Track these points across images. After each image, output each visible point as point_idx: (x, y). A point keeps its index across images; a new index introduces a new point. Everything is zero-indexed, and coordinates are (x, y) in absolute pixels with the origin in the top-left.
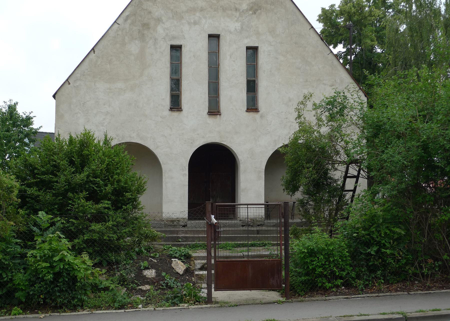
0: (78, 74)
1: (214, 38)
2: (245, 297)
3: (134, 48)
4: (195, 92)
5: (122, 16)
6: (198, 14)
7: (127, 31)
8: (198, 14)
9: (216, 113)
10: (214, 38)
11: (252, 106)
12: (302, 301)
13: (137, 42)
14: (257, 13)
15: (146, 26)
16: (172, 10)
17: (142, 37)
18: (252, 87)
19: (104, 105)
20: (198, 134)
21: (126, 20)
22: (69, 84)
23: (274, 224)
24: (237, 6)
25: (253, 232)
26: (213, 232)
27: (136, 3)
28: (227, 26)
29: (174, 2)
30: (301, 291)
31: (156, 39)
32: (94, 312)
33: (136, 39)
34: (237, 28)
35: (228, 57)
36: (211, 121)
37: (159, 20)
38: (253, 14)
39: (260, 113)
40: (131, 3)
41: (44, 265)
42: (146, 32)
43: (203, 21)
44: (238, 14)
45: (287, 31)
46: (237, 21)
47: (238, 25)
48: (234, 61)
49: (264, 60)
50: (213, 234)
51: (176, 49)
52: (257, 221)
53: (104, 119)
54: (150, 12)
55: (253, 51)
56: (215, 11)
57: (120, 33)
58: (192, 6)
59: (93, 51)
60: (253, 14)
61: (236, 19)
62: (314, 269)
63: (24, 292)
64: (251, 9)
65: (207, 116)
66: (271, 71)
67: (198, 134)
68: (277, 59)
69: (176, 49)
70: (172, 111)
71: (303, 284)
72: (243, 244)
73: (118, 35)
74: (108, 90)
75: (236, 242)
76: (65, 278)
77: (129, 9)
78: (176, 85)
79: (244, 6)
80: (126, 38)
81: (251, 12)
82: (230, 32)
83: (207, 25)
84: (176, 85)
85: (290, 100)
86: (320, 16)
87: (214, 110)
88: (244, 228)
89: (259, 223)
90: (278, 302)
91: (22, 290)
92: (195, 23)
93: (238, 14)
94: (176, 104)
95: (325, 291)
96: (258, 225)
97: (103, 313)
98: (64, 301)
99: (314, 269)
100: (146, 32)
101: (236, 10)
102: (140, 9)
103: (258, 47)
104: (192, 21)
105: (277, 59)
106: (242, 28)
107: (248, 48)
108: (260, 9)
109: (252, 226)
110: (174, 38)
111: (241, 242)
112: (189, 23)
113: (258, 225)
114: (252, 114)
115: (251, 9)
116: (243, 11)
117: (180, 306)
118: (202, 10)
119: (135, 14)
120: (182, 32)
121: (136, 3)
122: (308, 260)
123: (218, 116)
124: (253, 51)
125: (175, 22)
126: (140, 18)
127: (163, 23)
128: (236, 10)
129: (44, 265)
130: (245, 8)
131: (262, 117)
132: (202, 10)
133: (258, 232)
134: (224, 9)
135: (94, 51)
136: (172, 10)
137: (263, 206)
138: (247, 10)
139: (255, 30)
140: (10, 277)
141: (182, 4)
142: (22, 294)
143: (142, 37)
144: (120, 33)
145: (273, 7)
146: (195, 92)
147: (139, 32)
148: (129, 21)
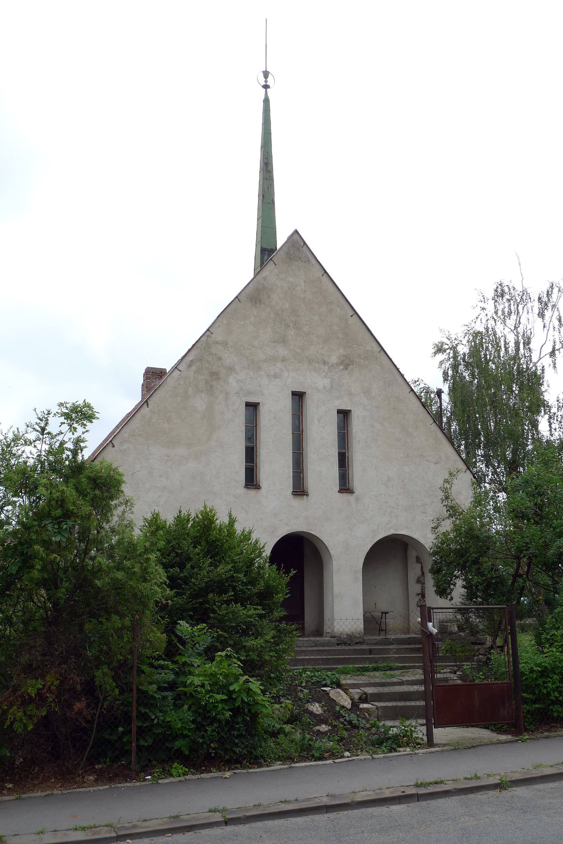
0: (125, 433)
1: (298, 397)
2: (476, 735)
3: (200, 403)
4: (275, 464)
5: (185, 360)
6: (279, 365)
7: (191, 381)
8: (279, 365)
9: (299, 493)
10: (298, 397)
11: (345, 487)
13: (203, 395)
14: (349, 369)
15: (215, 375)
16: (247, 358)
17: (210, 390)
18: (343, 460)
19: (160, 477)
20: (280, 520)
21: (190, 366)
22: (114, 446)
23: (376, 641)
24: (326, 358)
25: (363, 652)
26: (431, 645)
27: (202, 345)
28: (314, 382)
29: (249, 347)
30: (529, 725)
31: (227, 394)
32: (293, 765)
33: (202, 391)
34: (326, 385)
35: (316, 422)
36: (296, 502)
37: (231, 369)
38: (344, 369)
39: (355, 494)
40: (196, 345)
41: (219, 697)
42: (214, 383)
43: (286, 374)
44: (326, 368)
45: (384, 393)
46: (325, 377)
47: (327, 382)
48: (323, 427)
49: (357, 426)
50: (431, 648)
51: (252, 408)
52: (356, 637)
53: (160, 497)
54: (220, 359)
55: (344, 415)
56: (299, 362)
57: (182, 382)
58: (271, 355)
59: (146, 404)
60: (344, 369)
61: (324, 374)
62: (549, 694)
63: (187, 740)
64: (341, 364)
65: (292, 496)
66: (366, 442)
67: (280, 520)
68: (373, 427)
69: (252, 408)
70: (248, 488)
71: (532, 715)
72: (363, 667)
73: (179, 384)
74: (166, 458)
75: (355, 666)
76: (245, 717)
77: (193, 352)
78: (251, 454)
79: (334, 359)
80: (190, 389)
81: (342, 367)
82: (318, 391)
83: (289, 380)
84: (251, 454)
85: (389, 480)
87: (299, 490)
88: (339, 647)
89: (358, 641)
90: (511, 742)
91: (186, 736)
92: (276, 376)
93: (326, 368)
94: (252, 480)
96: (357, 643)
97: (306, 766)
98: (244, 751)
99: (549, 694)
100: (214, 383)
101: (324, 363)
102: (208, 353)
103: (350, 411)
104: (272, 373)
105: (373, 427)
106: (332, 386)
107: (339, 412)
108: (353, 365)
109: (350, 645)
110: (250, 393)
111: (361, 666)
112: (268, 376)
113: (357, 643)
114: (345, 496)
115: (341, 364)
116: (332, 365)
117: (400, 751)
118: (284, 360)
119: (201, 360)
120: (260, 386)
121: (202, 345)
122: (540, 681)
123: (305, 496)
124: (344, 415)
125: (251, 373)
126: (207, 365)
127: (237, 373)
128: (324, 363)
129: (219, 697)
130: (335, 362)
131: (357, 499)
132: (284, 360)
133: (371, 652)
134: (310, 362)
135: (147, 404)
136: (247, 358)
137: (451, 610)
138: (337, 364)
139: (346, 390)
140: (161, 718)
141: (259, 350)
142: (184, 742)
143: (210, 390)
144: (182, 382)
145: (367, 362)
146: (275, 464)
147: (207, 382)
148: (194, 368)
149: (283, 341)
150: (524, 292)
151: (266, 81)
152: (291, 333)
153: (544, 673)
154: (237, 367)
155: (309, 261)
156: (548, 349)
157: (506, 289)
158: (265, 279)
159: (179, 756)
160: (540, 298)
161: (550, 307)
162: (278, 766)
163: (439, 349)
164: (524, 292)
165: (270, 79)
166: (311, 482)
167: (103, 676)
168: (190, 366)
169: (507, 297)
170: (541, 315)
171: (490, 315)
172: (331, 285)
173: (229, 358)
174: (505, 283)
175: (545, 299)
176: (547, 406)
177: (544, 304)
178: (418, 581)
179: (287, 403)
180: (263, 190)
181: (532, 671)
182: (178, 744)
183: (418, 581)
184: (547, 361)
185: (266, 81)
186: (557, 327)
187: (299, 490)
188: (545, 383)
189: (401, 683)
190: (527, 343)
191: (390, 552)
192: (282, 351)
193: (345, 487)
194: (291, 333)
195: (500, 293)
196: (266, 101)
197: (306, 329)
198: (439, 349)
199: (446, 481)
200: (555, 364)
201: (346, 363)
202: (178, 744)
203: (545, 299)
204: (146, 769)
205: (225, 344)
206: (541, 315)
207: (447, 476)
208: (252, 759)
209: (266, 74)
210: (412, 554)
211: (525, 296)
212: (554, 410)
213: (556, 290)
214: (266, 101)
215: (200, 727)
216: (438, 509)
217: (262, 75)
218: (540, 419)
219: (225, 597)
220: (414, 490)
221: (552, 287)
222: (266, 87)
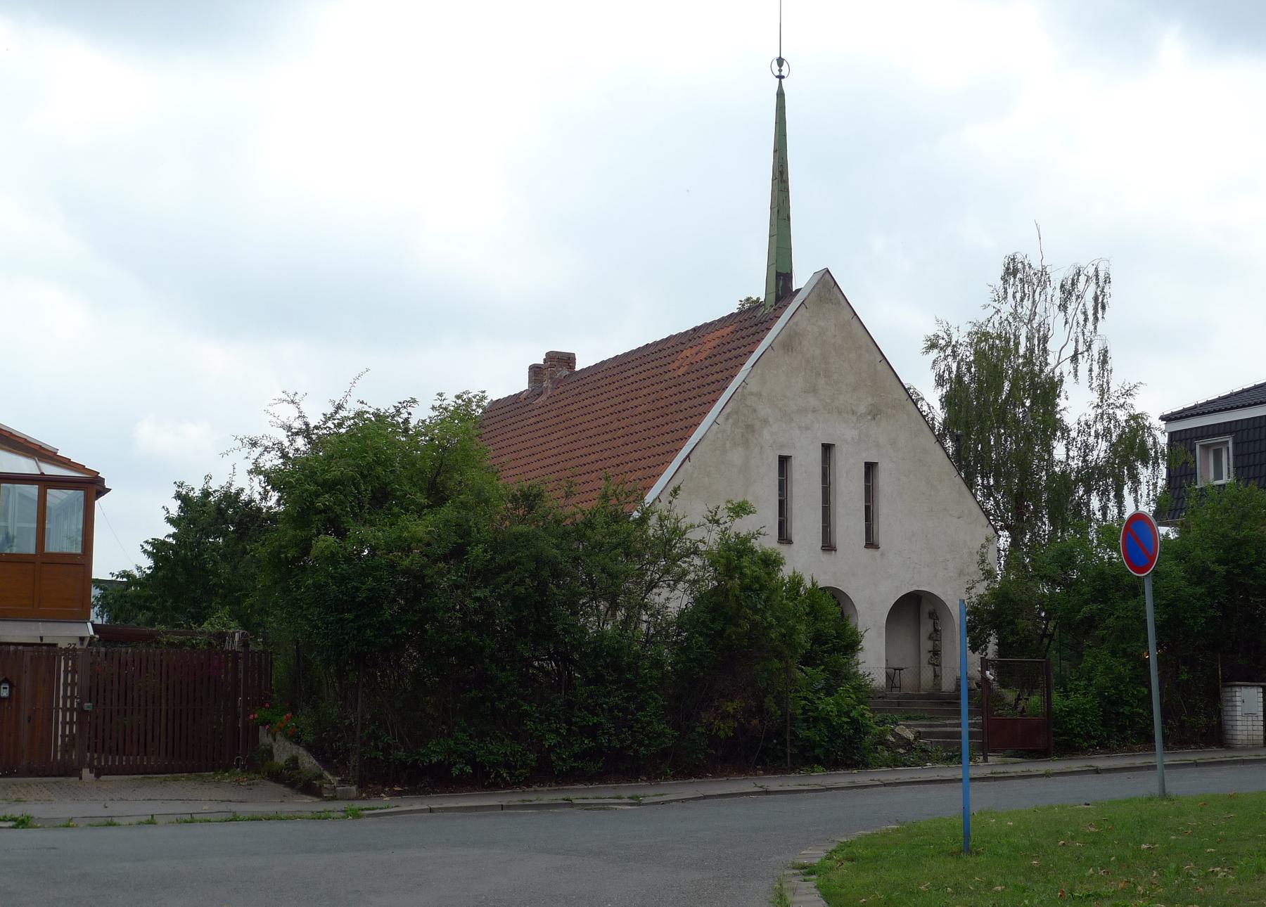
1: (827, 449)
3: (736, 456)
8: (809, 416)
11: (871, 543)
12: (603, 807)
15: (750, 428)
17: (746, 443)
21: (727, 419)
28: (843, 433)
36: (825, 557)
37: (765, 421)
44: (855, 419)
47: (855, 433)
49: (884, 479)
51: (784, 461)
55: (870, 468)
57: (720, 435)
69: (784, 461)
86: (568, 359)
92: (807, 428)
93: (855, 419)
95: (495, 785)
101: (853, 413)
110: (782, 446)
114: (871, 552)
124: (870, 468)
128: (853, 413)
131: (882, 555)
134: (840, 412)
143: (746, 443)
149: (814, 390)
150: (1043, 271)
151: (780, 71)
152: (822, 381)
153: (1071, 712)
154: (771, 420)
155: (839, 303)
156: (1069, 351)
157: (1020, 266)
158: (797, 324)
159: (818, 761)
160: (1062, 286)
161: (1074, 298)
162: (884, 769)
163: (933, 345)
164: (1043, 271)
165: (785, 67)
166: (839, 537)
167: (770, 703)
168: (727, 419)
169: (1019, 276)
170: (1063, 307)
171: (1004, 317)
172: (861, 328)
173: (764, 410)
174: (1019, 258)
175: (1068, 287)
176: (1065, 431)
177: (1068, 291)
178: (930, 638)
179: (818, 455)
180: (779, 205)
181: (1061, 710)
182: (817, 751)
183: (930, 638)
184: (1067, 367)
185: (780, 71)
186: (1082, 323)
187: (828, 546)
188: (1062, 394)
189: (945, 726)
190: (1045, 339)
191: (914, 609)
192: (813, 401)
193: (871, 543)
194: (822, 381)
195: (1011, 271)
196: (781, 95)
197: (835, 377)
198: (933, 345)
199: (983, 546)
200: (1076, 371)
201: (874, 413)
202: (817, 751)
203: (1068, 287)
204: (792, 770)
205: (759, 395)
206: (1063, 307)
207: (983, 541)
208: (863, 765)
209: (780, 61)
210: (926, 608)
211: (1043, 277)
212: (1073, 434)
213: (1082, 279)
214: (781, 95)
215: (831, 741)
216: (974, 571)
217: (775, 63)
218: (1055, 443)
219: (824, 648)
220: (942, 544)
221: (1078, 274)
222: (781, 77)
